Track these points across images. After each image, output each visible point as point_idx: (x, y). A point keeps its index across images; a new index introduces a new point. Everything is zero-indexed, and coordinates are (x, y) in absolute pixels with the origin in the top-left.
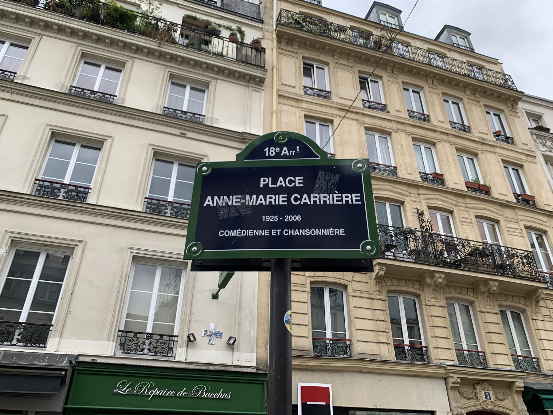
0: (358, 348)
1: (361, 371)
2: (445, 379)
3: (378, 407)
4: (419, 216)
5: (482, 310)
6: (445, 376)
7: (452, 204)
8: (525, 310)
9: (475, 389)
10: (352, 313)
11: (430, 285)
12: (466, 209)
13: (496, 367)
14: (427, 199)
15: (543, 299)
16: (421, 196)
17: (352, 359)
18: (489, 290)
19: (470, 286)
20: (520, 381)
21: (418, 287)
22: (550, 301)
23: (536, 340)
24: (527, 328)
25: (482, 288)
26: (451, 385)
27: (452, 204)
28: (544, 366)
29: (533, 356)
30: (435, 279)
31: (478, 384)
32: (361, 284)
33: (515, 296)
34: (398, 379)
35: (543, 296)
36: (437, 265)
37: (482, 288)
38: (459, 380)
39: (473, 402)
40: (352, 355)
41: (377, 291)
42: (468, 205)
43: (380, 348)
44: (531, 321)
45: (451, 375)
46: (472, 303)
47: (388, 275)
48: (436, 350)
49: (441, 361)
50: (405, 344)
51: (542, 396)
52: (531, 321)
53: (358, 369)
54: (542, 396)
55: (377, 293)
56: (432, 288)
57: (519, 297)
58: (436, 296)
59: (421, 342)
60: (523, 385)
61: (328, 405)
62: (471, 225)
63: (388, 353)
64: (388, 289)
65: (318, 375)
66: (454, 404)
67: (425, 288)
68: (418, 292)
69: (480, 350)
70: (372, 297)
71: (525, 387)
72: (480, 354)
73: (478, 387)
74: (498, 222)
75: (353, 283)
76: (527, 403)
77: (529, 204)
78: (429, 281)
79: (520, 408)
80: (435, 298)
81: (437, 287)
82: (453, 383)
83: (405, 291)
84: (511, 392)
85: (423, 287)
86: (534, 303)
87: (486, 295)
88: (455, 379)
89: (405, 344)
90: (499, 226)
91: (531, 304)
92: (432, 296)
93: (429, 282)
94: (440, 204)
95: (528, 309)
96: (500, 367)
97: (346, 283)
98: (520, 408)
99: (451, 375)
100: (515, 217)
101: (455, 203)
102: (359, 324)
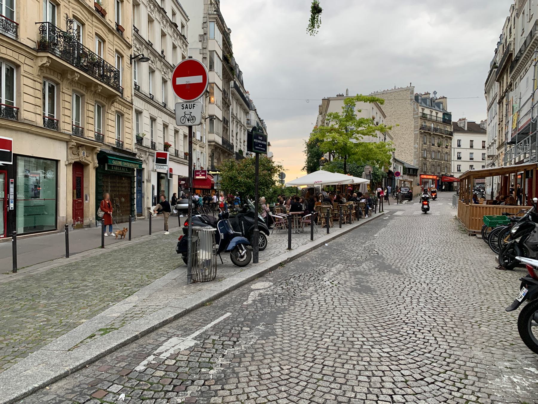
0: (25, 115)
1: (28, 132)
2: (67, 142)
3: (34, 156)
4: (67, 21)
5: (88, 102)
6: (68, 140)
7: (85, 18)
8: (105, 106)
9: (78, 149)
10: (22, 89)
11: (91, 91)
12: (91, 25)
13: (88, 138)
14: (73, 8)
15: (116, 102)
16: (70, 4)
17: (17, 121)
18: (96, 91)
19: (85, 85)
20: (100, 147)
21: (60, 79)
22: (5, 48)
23: (85, 116)
24: (102, 117)
25: (69, 76)
26: (71, 146)
27: (85, 18)
28: (86, 133)
29: (101, 133)
30: (73, 77)
31: (81, 147)
32: (29, 67)
33: (56, 71)
34: (45, 139)
35: (117, 100)
36: (76, 67)
37: (93, 89)
38: (75, 144)
39: (76, 157)
40: (19, 118)
41: (38, 75)
42: (94, 23)
43: (36, 117)
44: (61, 93)
45: (73, 141)
46: (83, 95)
47: (79, 82)
48: (63, 123)
49: (66, 131)
50: (2, 103)
51: (109, 157)
52: (61, 93)
53: (27, 130)
54: (109, 157)
55: (38, 77)
56: (68, 82)
57: (105, 97)
58: (69, 88)
59: (13, 103)
60: (100, 150)
61: (11, 152)
62: (92, 39)
63: (40, 121)
64: (44, 76)
65: (8, 132)
66: (70, 157)
67: (64, 80)
68: (59, 82)
69: (80, 126)
70: (35, 79)
71: (100, 151)
72: (15, 109)
73: (80, 148)
74: (104, 41)
75: (25, 65)
76: (98, 159)
77: (119, 32)
78: (69, 76)
79: (95, 162)
80: (68, 89)
81: (72, 82)
82: (72, 145)
83: (52, 79)
84: (92, 153)
85: (63, 79)
86: (111, 103)
87: (93, 93)
88: (74, 143)
89: (2, 103)
90: (104, 45)
91: (109, 103)
92: (67, 87)
93: (68, 77)
94: (79, 16)
95: (107, 106)
96: (90, 138)
97: (20, 64)
98: (95, 162)
99: (73, 141)
100: (112, 41)
101: (87, 18)
102: (26, 98)
